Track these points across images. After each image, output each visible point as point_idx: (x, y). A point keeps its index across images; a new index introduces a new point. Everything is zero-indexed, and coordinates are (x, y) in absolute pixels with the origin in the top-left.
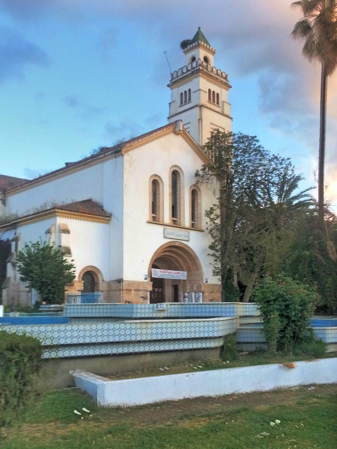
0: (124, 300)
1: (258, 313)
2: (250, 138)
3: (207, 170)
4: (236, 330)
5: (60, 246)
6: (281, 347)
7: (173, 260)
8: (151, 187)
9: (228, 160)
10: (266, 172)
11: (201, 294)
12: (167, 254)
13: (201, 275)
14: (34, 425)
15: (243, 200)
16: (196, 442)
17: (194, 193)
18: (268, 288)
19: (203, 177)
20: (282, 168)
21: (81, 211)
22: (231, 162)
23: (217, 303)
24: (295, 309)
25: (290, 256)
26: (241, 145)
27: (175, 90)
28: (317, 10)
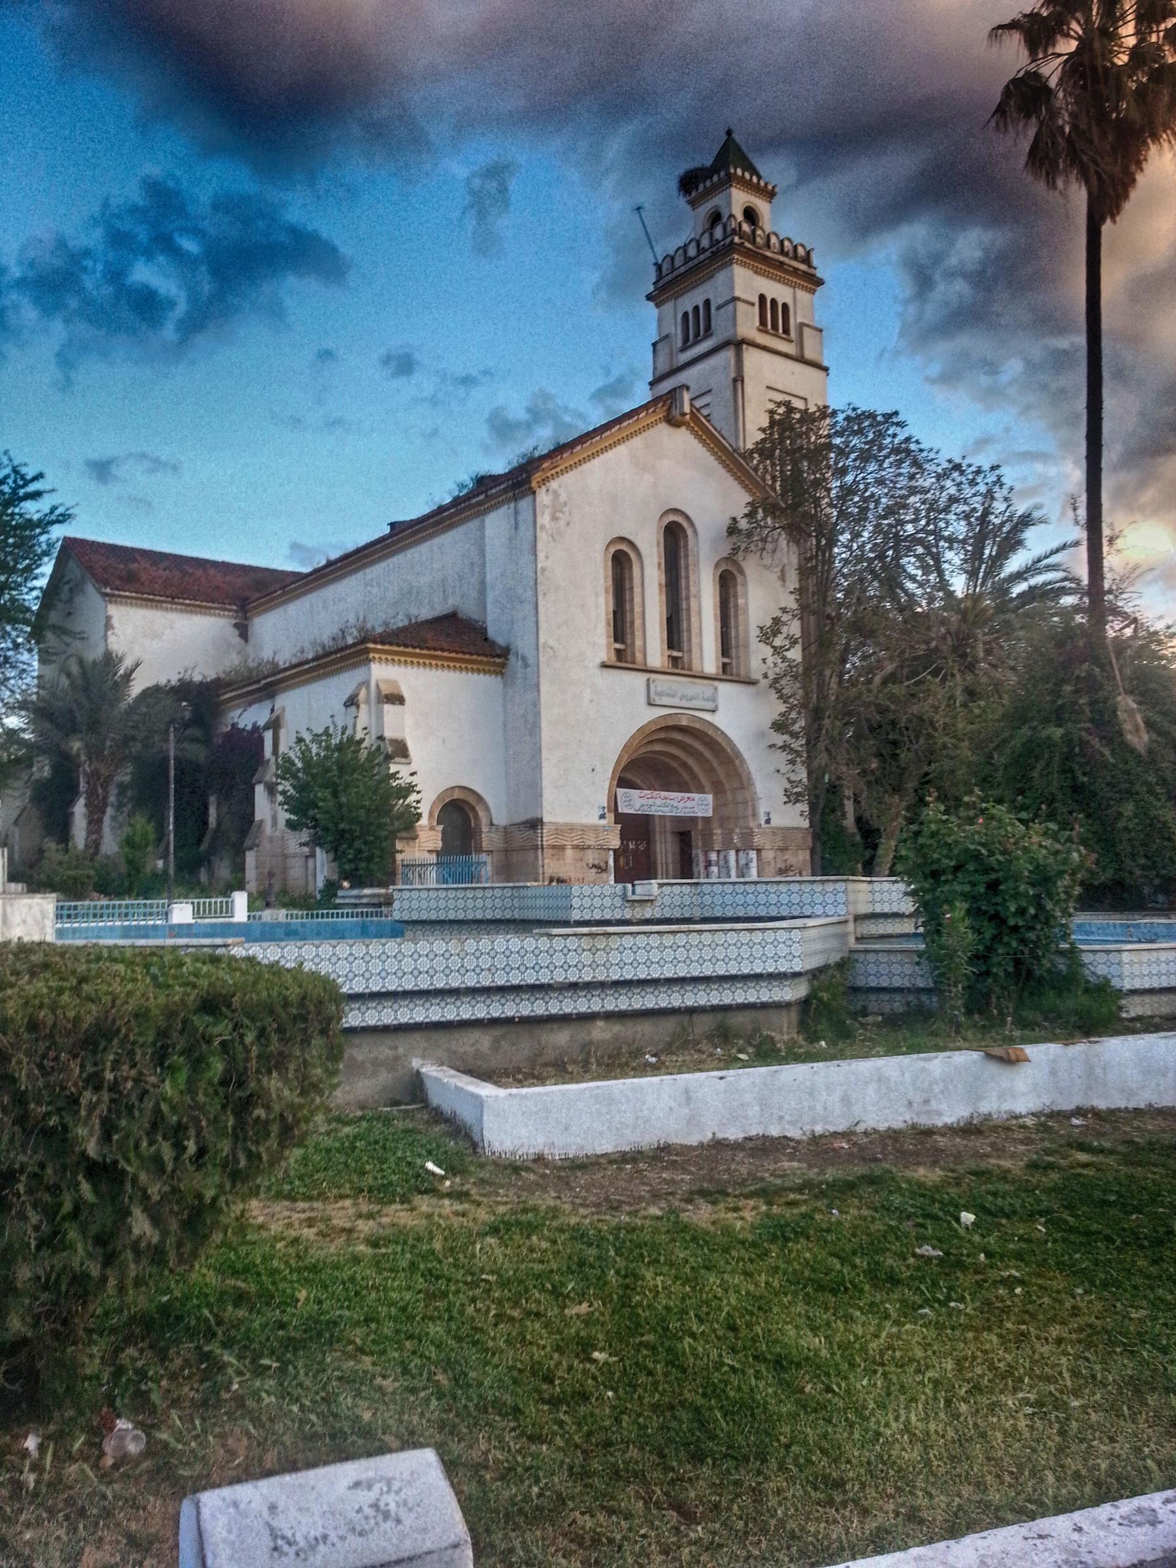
0: (547, 875)
1: (908, 906)
2: (879, 418)
3: (760, 515)
4: (846, 955)
5: (381, 738)
6: (977, 1003)
7: (674, 764)
8: (610, 573)
9: (817, 484)
10: (929, 511)
11: (753, 854)
12: (658, 747)
13: (750, 803)
14: (301, 1205)
15: (865, 591)
16: (729, 1268)
17: (727, 582)
18: (933, 835)
19: (749, 534)
20: (974, 495)
21: (431, 644)
22: (829, 490)
23: (798, 878)
24: (1016, 895)
25: (1005, 741)
26: (855, 441)
27: (668, 307)
28: (1068, 36)
